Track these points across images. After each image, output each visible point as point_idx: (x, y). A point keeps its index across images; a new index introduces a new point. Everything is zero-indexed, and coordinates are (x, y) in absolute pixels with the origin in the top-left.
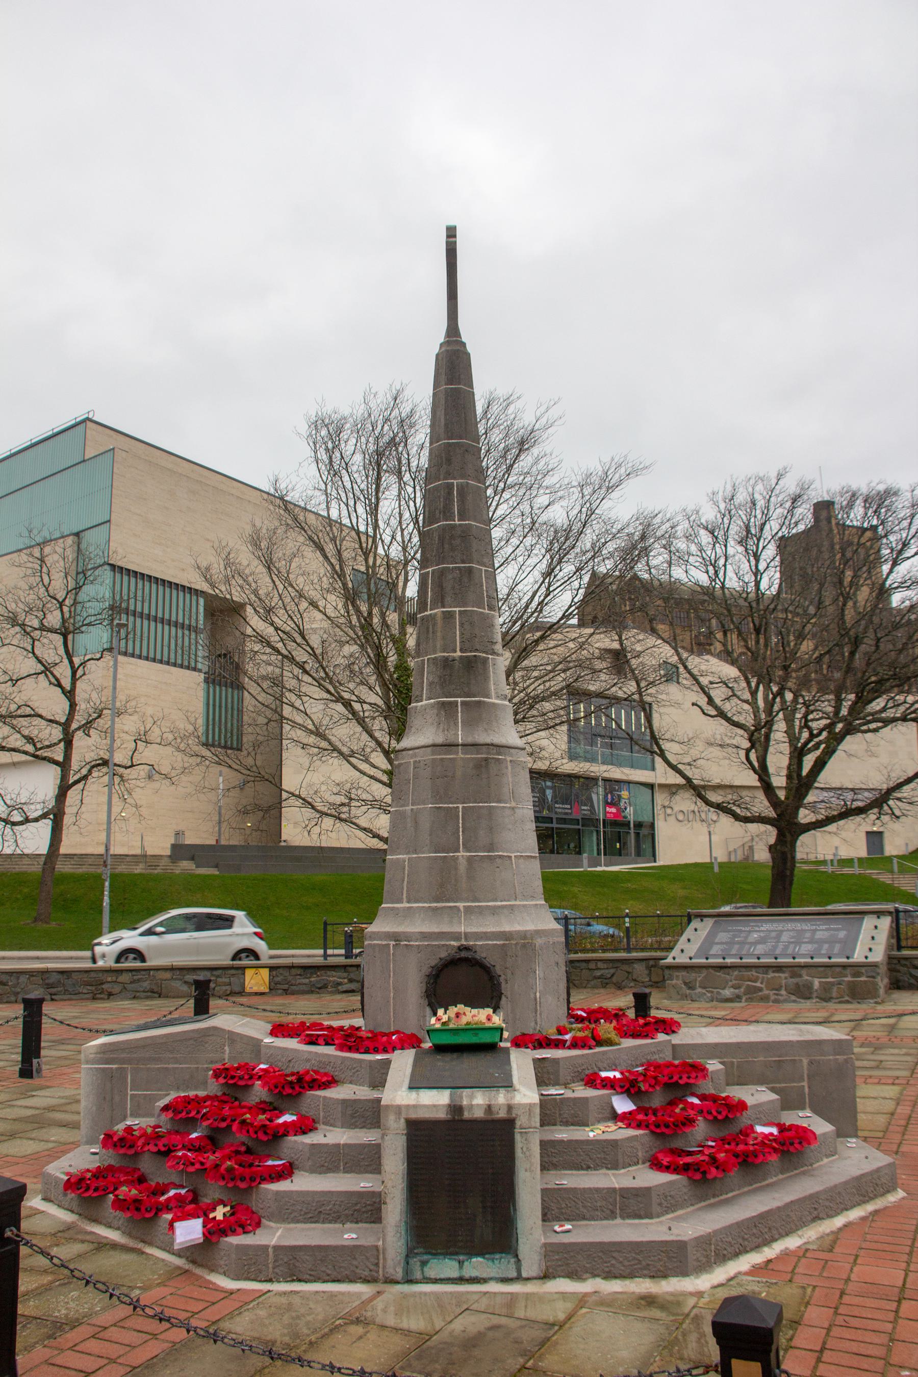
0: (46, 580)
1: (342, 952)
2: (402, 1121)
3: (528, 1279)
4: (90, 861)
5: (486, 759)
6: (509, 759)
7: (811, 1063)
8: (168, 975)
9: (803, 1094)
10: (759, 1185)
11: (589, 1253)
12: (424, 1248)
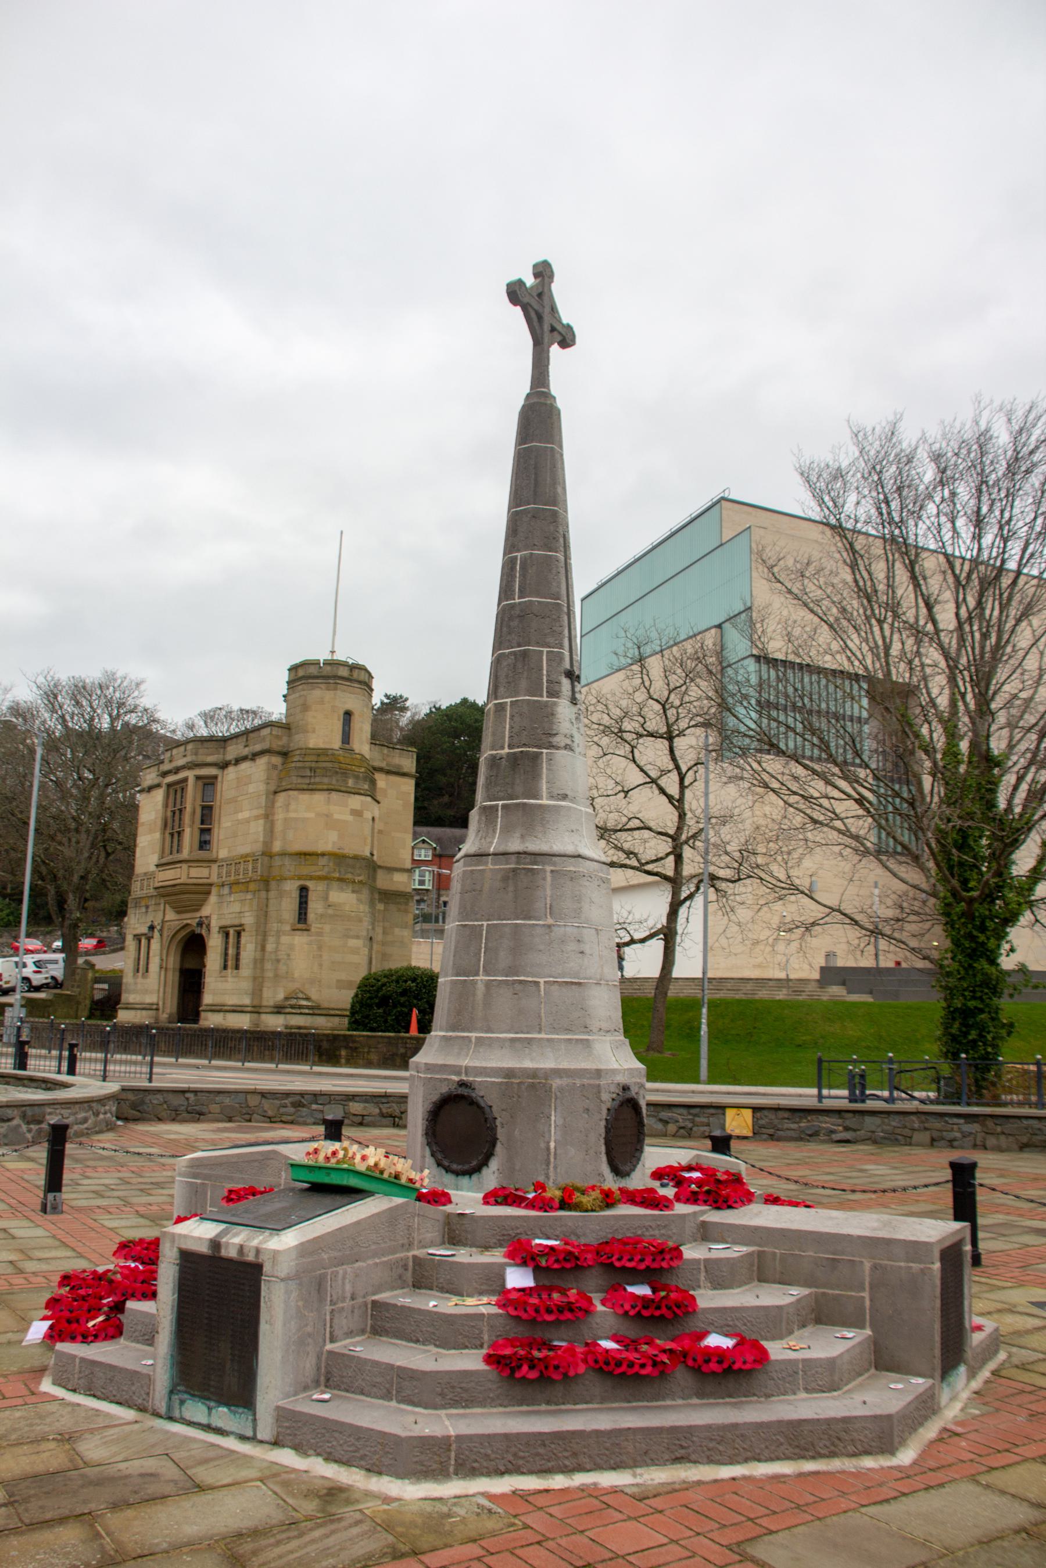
0: (647, 684)
1: (845, 1093)
2: (175, 1250)
3: (261, 1442)
4: (729, 985)
5: (514, 870)
6: (548, 868)
7: (875, 1267)
9: (862, 1308)
10: (645, 1404)
11: (314, 1427)
12: (187, 1386)
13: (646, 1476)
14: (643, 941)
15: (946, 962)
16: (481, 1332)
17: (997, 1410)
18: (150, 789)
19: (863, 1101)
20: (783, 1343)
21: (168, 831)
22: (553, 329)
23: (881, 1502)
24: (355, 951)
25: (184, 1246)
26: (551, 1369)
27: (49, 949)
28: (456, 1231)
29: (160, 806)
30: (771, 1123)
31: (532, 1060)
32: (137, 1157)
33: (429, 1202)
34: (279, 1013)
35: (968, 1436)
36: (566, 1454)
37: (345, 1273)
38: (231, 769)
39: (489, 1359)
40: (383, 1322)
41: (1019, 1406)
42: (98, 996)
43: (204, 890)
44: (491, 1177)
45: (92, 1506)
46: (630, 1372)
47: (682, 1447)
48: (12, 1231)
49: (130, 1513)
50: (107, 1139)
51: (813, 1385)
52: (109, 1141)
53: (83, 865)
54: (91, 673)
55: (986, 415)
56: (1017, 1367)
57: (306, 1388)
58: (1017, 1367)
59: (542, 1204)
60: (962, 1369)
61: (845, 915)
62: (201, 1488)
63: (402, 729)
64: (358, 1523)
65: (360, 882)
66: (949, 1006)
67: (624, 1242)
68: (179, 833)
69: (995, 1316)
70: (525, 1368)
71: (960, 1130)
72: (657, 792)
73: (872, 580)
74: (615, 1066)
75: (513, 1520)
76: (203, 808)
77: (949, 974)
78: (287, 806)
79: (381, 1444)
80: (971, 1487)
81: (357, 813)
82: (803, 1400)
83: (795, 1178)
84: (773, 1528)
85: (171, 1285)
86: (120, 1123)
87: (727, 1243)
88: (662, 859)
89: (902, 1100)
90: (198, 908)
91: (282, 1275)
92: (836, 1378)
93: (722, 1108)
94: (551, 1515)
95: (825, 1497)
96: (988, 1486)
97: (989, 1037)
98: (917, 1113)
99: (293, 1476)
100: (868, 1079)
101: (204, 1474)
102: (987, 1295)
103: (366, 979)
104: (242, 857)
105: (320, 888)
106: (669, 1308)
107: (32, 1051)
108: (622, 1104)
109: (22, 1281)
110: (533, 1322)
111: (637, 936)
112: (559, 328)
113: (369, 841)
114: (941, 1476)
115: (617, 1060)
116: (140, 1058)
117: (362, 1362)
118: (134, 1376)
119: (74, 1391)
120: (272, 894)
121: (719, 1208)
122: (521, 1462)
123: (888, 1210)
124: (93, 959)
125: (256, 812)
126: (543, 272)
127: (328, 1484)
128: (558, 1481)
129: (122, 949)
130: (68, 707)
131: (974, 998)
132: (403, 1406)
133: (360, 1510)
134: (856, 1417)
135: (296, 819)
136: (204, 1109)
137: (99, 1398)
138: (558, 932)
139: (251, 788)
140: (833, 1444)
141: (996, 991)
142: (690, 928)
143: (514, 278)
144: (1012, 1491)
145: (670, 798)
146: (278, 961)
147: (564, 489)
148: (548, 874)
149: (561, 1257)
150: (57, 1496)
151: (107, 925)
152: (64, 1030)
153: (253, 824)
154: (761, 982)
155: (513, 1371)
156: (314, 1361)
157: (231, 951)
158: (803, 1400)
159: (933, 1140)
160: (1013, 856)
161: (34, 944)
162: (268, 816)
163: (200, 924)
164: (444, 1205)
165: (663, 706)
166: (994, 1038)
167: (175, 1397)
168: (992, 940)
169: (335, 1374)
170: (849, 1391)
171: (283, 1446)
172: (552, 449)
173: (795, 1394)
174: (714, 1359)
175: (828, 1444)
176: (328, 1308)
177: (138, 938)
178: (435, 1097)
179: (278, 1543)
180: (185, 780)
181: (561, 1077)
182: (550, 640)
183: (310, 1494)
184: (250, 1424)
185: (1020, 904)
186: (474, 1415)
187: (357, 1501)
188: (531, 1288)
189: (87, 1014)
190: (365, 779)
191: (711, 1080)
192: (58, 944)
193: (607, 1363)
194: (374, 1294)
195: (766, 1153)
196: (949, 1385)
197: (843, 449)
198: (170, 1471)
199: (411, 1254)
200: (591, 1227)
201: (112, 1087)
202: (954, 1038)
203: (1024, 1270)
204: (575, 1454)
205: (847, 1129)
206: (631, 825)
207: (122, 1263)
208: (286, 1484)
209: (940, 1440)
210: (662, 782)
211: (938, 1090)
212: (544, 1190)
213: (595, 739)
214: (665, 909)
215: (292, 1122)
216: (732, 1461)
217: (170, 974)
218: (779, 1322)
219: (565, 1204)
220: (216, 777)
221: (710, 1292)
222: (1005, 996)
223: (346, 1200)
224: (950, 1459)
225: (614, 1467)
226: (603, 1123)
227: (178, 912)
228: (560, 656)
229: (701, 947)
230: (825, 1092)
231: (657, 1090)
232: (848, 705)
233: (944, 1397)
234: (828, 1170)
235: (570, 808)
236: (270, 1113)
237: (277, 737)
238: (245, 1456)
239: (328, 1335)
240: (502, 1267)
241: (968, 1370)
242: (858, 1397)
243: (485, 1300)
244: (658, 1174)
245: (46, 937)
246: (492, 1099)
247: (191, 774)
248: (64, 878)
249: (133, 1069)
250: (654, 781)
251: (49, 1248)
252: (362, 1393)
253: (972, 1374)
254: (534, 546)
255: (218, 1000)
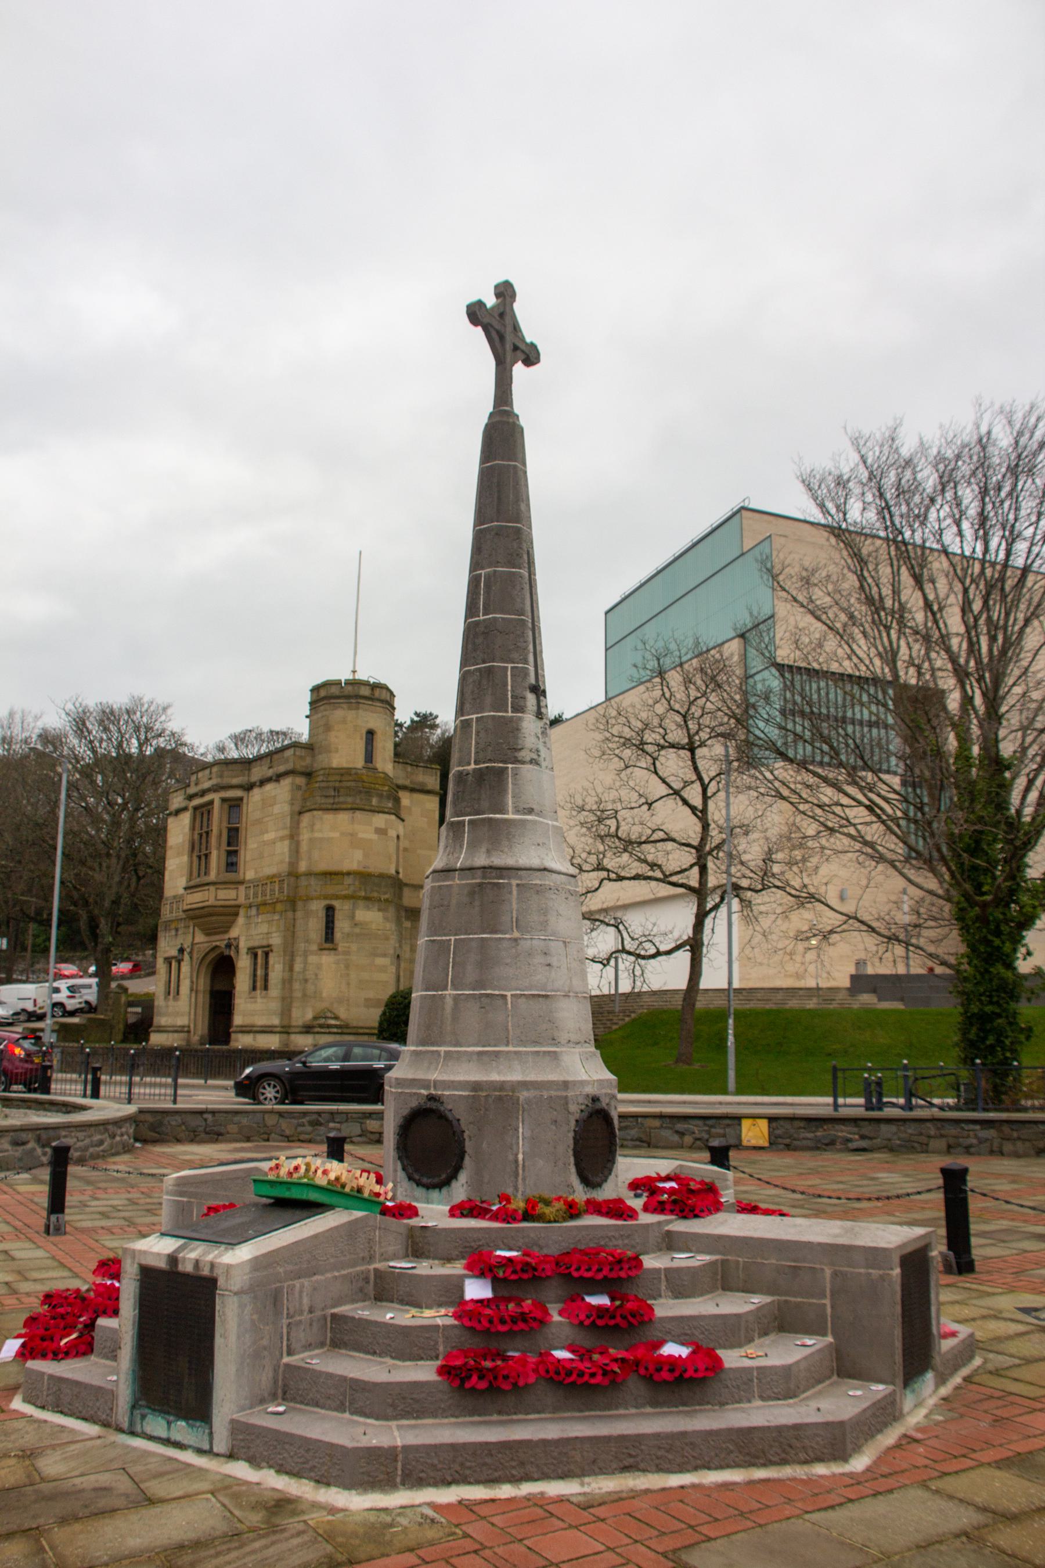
0: (667, 695)
1: (861, 1101)
3: (217, 1455)
4: (759, 995)
5: (480, 885)
6: (514, 882)
7: (835, 1274)
8: (657, 1123)
9: (824, 1316)
10: (598, 1413)
13: (594, 1485)
14: (669, 952)
15: (962, 967)
16: (437, 1343)
17: (962, 1416)
18: (178, 812)
19: (880, 1109)
20: (742, 1352)
21: (195, 854)
22: (516, 348)
23: (825, 1509)
24: (383, 969)
25: (143, 1262)
26: (500, 1378)
27: (86, 974)
28: (419, 1244)
29: (187, 829)
30: (787, 1133)
31: (499, 1073)
32: (149, 1179)
33: (394, 1216)
34: (307, 1032)
35: (927, 1442)
36: (514, 1464)
37: (302, 1286)
38: (256, 791)
39: (442, 1371)
40: (342, 1335)
41: (986, 1412)
42: (131, 1020)
43: (231, 912)
44: (460, 1191)
45: (41, 1521)
46: (580, 1381)
47: (630, 1455)
48: (12, 1253)
49: (77, 1527)
50: (121, 1163)
51: (769, 1393)
52: (124, 1163)
53: (114, 890)
54: (119, 699)
55: (987, 418)
56: (990, 1372)
57: (262, 1401)
58: (990, 1372)
59: (506, 1216)
60: (930, 1376)
61: (862, 922)
62: (151, 1501)
63: (432, 747)
64: (299, 1533)
65: (386, 900)
66: (966, 1012)
67: (583, 1252)
68: (206, 855)
69: (979, 1322)
70: (475, 1378)
71: (976, 1137)
72: (680, 803)
73: (877, 585)
74: (584, 1077)
75: (454, 1529)
76: (230, 830)
77: (966, 979)
78: (312, 827)
79: (330, 1455)
80: (920, 1493)
81: (381, 832)
82: (758, 1408)
83: (801, 1189)
84: (712, 1535)
85: (132, 1301)
86: (138, 1145)
87: (691, 1251)
88: (686, 870)
89: (921, 1107)
90: (227, 929)
91: (235, 1288)
92: (792, 1386)
93: (738, 1119)
94: (493, 1524)
95: (770, 1503)
96: (937, 1492)
97: (1007, 1042)
98: (933, 1120)
99: (244, 1488)
100: (885, 1088)
101: (156, 1488)
102: (975, 1302)
103: (393, 997)
104: (268, 878)
105: (346, 907)
106: (624, 1318)
107: (103, 1078)
108: (591, 1115)
109: (15, 1301)
110: (487, 1333)
111: (663, 948)
112: (522, 347)
113: (395, 857)
114: (891, 1482)
115: (586, 1071)
116: (75, 1076)
117: (318, 1374)
118: (98, 1391)
119: (43, 1407)
120: (299, 914)
121: (685, 1217)
122: (468, 1472)
123: (892, 1219)
124: (126, 983)
125: (281, 833)
126: (505, 292)
127: (277, 1496)
128: (506, 1491)
129: (153, 973)
130: (95, 730)
131: (991, 1003)
132: (356, 1418)
133: (305, 1521)
134: (807, 1424)
135: (321, 839)
136: (222, 1130)
137: (66, 1414)
138: (525, 945)
139: (276, 809)
140: (784, 1451)
141: (1014, 996)
142: (715, 940)
143: (474, 299)
144: (961, 1495)
145: (693, 809)
146: (306, 981)
147: (528, 506)
148: (514, 888)
149: (519, 1268)
150: (24, 1509)
151: (143, 949)
152: (88, 1054)
153: (278, 844)
154: (792, 992)
155: (463, 1381)
156: (271, 1374)
157: (259, 972)
158: (758, 1408)
159: (949, 1147)
160: (1027, 860)
161: (69, 969)
162: (293, 836)
163: (229, 946)
164: (410, 1217)
165: (684, 717)
166: (1012, 1043)
167: (137, 1412)
168: (1008, 944)
169: (292, 1388)
170: (807, 1398)
171: (238, 1459)
172: (515, 467)
173: (749, 1401)
174: (666, 1368)
175: (779, 1451)
176: (285, 1322)
177: (168, 961)
178: (406, 1112)
179: (218, 1554)
180: (211, 802)
181: (528, 1090)
182: (515, 655)
183: (257, 1505)
184: (206, 1437)
185: (1034, 907)
186: (424, 1426)
187: (303, 1512)
188: (488, 1300)
189: (115, 1037)
190: (388, 798)
191: (739, 1092)
192: (92, 969)
193: (558, 1373)
194: (334, 1307)
195: (782, 1163)
196: (913, 1391)
197: (843, 457)
198: (124, 1484)
199: (372, 1267)
200: (553, 1237)
201: (131, 1109)
202: (972, 1044)
203: (1018, 1275)
204: (522, 1464)
205: (863, 1137)
206: (655, 837)
207: (99, 1280)
208: (236, 1497)
209: (898, 1446)
210: (685, 794)
211: (958, 1097)
212: (509, 1201)
213: (617, 752)
214: (691, 920)
215: (310, 1141)
216: (681, 1469)
217: (201, 996)
218: (738, 1332)
219: (528, 1215)
220: (241, 799)
221: (671, 1302)
222: (1023, 1000)
223: (305, 1213)
224: (905, 1465)
225: (563, 1476)
226: (571, 1135)
227: (207, 935)
228: (525, 673)
229: (726, 958)
230: (841, 1101)
231: (684, 1103)
232: (857, 709)
233: (908, 1402)
234: (839, 1179)
235: (535, 822)
236: (288, 1132)
237: (301, 757)
238: (201, 1469)
239: (285, 1348)
240: (461, 1278)
241: (936, 1377)
242: (814, 1404)
243: (443, 1311)
244: (635, 1186)
245: (82, 963)
246: (461, 1113)
247: (216, 797)
248: (96, 903)
249: (157, 1091)
250: (676, 793)
251: (47, 1269)
252: (317, 1405)
253: (941, 1380)
254: (497, 564)
255: (248, 1021)
